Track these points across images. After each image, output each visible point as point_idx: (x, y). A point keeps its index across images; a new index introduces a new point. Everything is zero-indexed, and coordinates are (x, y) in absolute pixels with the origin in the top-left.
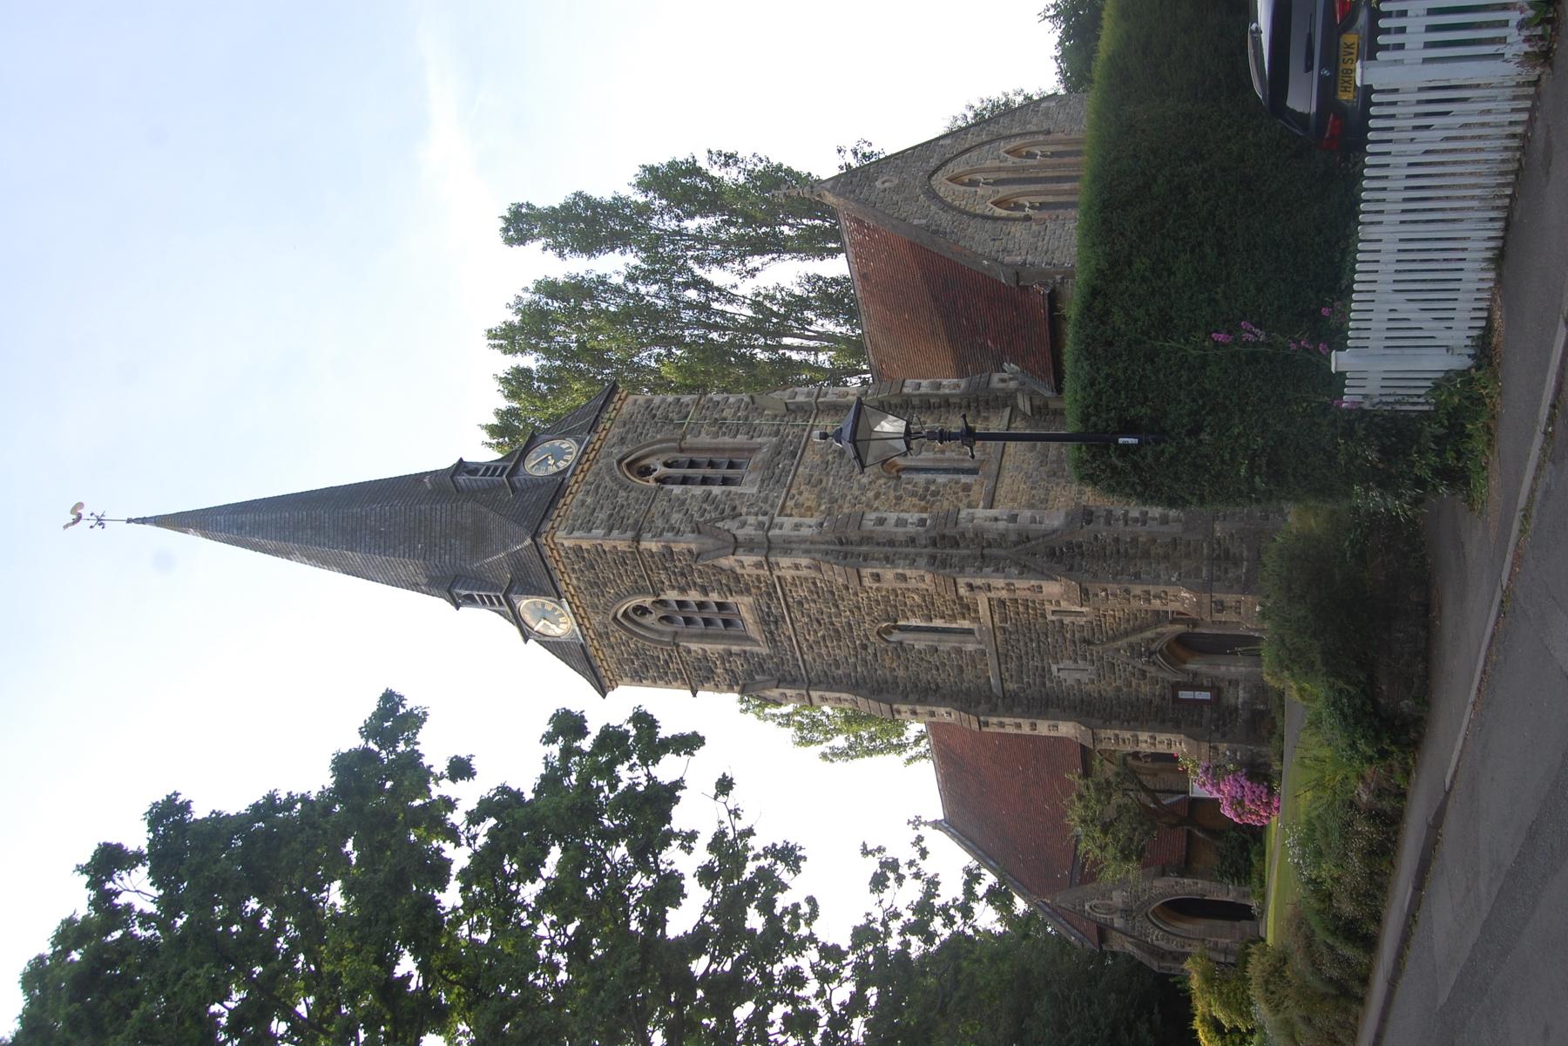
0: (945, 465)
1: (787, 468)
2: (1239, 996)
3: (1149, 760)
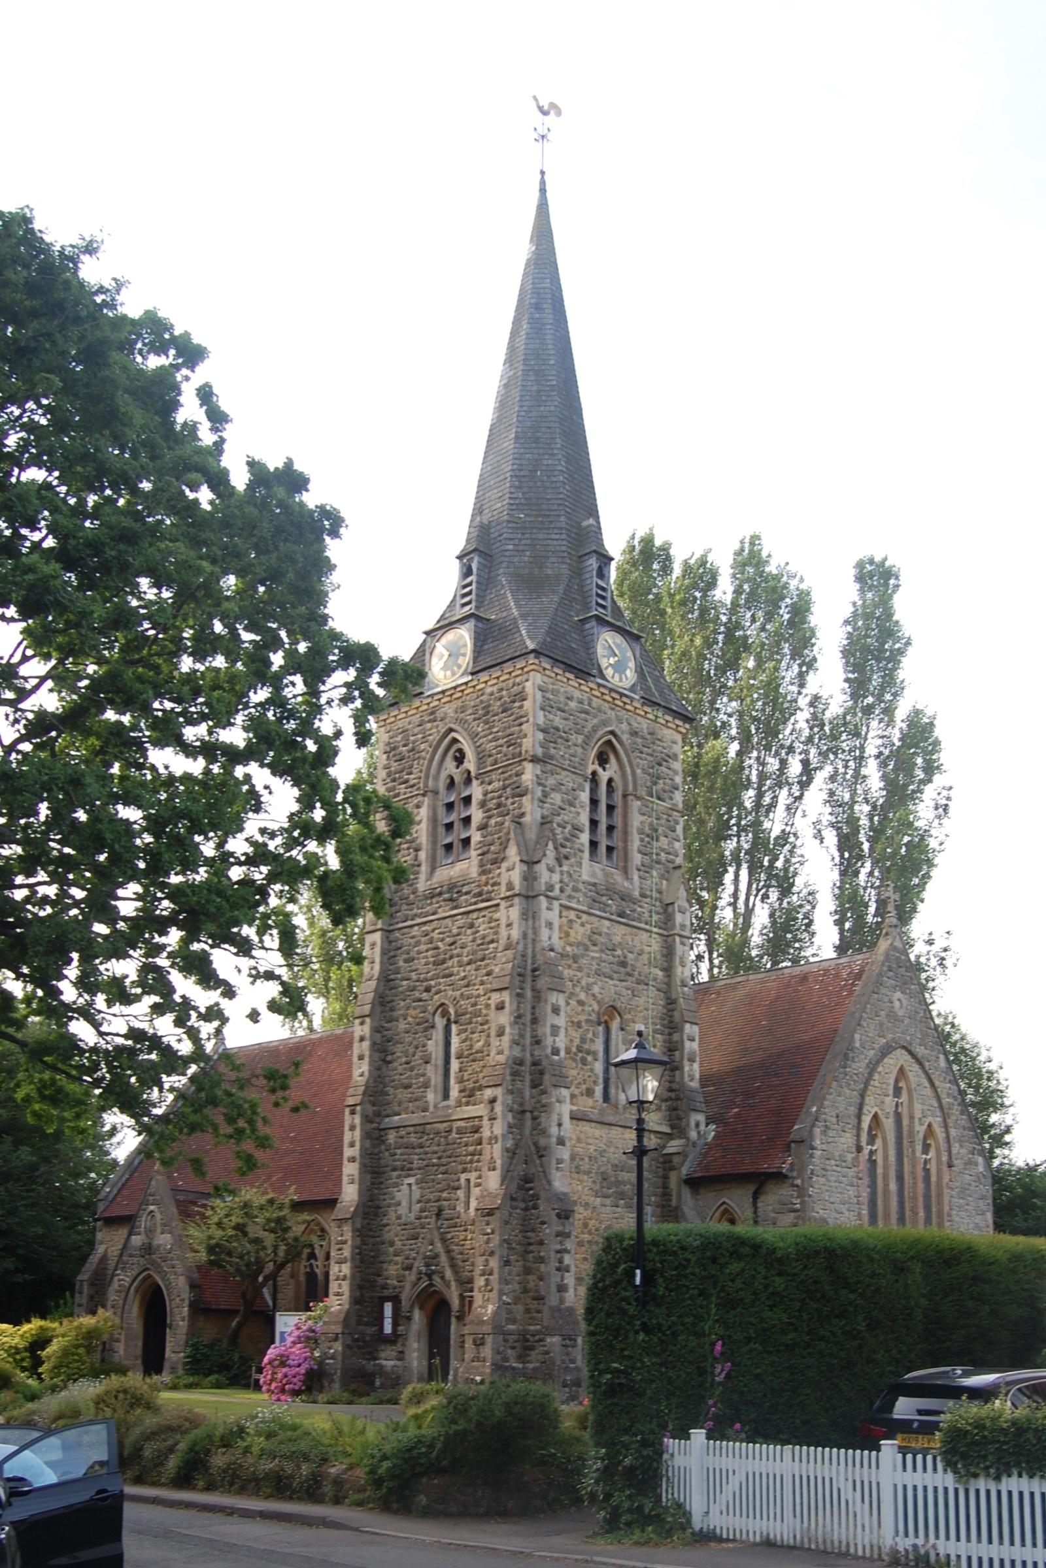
3: (308, 1270)
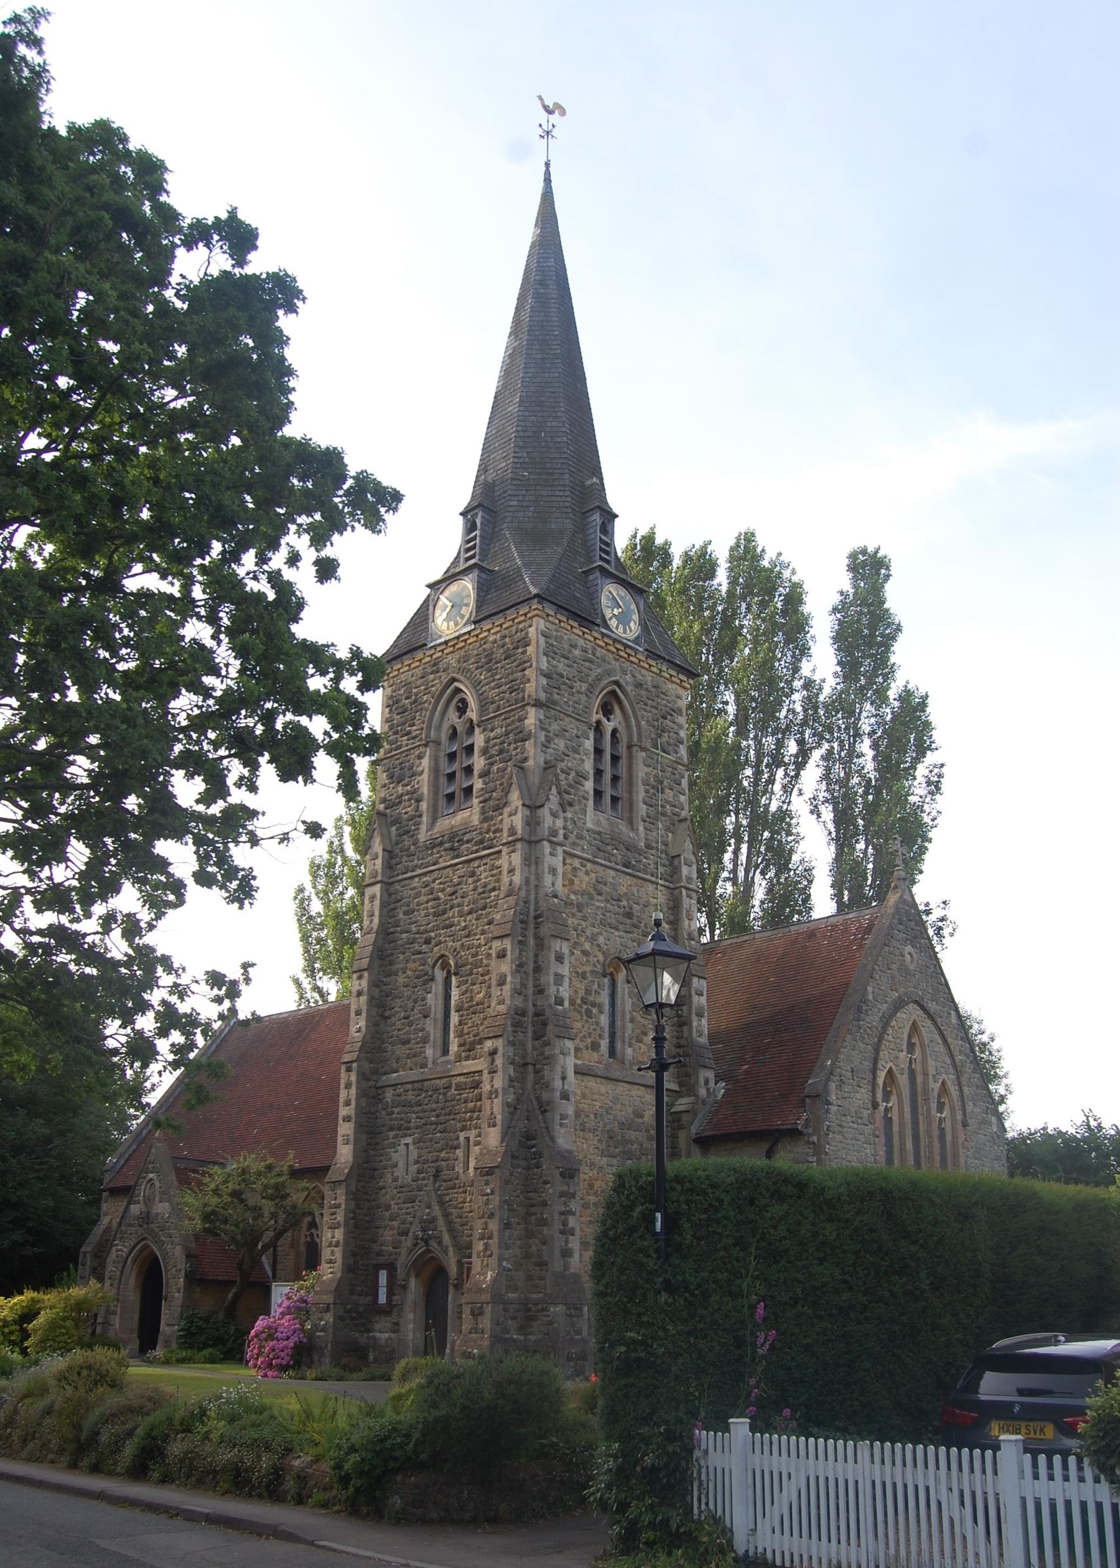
0: (619, 1023)
1: (613, 859)
2: (62, 1338)
3: (309, 1239)
